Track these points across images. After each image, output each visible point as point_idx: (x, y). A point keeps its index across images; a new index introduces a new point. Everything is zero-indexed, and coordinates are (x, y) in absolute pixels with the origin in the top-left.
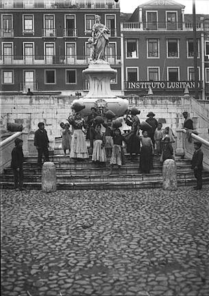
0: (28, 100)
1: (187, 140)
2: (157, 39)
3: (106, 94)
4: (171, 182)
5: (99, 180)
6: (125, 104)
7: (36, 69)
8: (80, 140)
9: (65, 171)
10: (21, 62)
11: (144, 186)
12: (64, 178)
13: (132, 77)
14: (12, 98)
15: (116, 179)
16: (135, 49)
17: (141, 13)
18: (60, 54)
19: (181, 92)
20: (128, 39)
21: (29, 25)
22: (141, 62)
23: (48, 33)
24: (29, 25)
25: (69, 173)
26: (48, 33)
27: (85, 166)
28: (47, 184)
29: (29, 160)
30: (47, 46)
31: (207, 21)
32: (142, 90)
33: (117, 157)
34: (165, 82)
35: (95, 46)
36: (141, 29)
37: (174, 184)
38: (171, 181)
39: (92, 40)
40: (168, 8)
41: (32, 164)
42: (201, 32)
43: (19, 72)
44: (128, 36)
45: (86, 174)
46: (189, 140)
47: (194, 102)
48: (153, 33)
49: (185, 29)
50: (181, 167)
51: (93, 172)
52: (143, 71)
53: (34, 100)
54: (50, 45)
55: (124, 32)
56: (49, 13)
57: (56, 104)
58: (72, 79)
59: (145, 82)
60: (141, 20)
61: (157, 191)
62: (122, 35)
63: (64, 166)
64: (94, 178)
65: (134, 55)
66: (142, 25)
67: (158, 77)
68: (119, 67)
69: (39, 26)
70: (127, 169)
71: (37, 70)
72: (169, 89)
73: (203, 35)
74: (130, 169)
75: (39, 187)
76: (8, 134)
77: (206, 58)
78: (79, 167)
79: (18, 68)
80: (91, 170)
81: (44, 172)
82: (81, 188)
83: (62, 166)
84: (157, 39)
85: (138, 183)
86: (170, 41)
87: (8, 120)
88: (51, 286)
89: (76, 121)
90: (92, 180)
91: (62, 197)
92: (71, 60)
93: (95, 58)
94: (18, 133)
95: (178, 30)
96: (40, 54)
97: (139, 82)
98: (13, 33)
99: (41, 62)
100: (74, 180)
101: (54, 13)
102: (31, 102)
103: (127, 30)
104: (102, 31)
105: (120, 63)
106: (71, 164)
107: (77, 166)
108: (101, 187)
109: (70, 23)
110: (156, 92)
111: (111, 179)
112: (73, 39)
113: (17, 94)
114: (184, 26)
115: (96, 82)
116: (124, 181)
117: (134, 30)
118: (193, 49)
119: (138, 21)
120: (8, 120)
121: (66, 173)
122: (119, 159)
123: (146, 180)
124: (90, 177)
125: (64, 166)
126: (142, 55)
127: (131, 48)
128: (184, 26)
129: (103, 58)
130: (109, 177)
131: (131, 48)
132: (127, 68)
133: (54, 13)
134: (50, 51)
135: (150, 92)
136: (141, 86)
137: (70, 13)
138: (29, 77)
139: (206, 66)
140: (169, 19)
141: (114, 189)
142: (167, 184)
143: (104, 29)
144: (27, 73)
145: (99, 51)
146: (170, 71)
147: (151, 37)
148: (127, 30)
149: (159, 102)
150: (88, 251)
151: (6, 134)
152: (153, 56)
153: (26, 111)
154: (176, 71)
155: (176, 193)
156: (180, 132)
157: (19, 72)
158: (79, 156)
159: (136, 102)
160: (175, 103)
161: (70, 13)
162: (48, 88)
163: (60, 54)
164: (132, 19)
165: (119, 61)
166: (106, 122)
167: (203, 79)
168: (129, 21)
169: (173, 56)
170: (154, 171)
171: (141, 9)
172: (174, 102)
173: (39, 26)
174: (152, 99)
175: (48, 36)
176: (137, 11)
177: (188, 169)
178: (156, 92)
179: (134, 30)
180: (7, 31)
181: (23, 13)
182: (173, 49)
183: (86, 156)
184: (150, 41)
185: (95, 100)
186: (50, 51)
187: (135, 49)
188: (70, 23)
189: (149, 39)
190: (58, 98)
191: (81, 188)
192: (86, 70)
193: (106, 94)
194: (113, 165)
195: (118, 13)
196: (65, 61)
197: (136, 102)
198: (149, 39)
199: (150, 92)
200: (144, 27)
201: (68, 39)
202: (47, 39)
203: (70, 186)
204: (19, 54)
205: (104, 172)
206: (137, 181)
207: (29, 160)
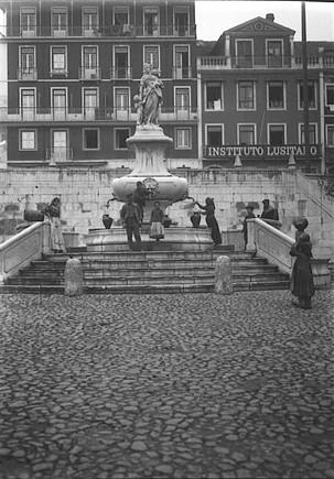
0: (57, 175)
3: (158, 171)
6: (183, 185)
9: (96, 271)
10: (47, 117)
11: (193, 290)
12: (95, 280)
13: (214, 138)
14: (34, 173)
16: (219, 97)
17: (228, 42)
18: (106, 104)
19: (284, 161)
20: (207, 82)
21: (59, 62)
23: (88, 73)
24: (59, 62)
26: (88, 73)
28: (71, 286)
29: (52, 259)
30: (87, 92)
31: (329, 54)
34: (264, 147)
35: (144, 105)
36: (228, 67)
40: (269, 34)
41: (56, 263)
42: (318, 71)
43: (44, 131)
44: (209, 78)
45: (123, 275)
47: (300, 177)
48: (246, 73)
49: (294, 66)
50: (248, 268)
53: (65, 175)
54: (91, 92)
55: (202, 72)
56: (88, 43)
57: (97, 180)
58: (91, 142)
60: (227, 53)
62: (199, 76)
64: (132, 279)
65: (218, 106)
66: (229, 61)
67: (254, 138)
69: (74, 65)
71: (72, 129)
73: (321, 75)
74: (179, 270)
75: (62, 291)
76: (25, 224)
77: (327, 110)
79: (44, 127)
81: (68, 270)
82: (115, 291)
85: (188, 286)
87: (27, 203)
88: (64, 405)
92: (122, 115)
94: (38, 223)
95: (285, 67)
96: (75, 104)
97: (225, 146)
98: (36, 74)
99: (79, 117)
101: (96, 43)
102: (61, 178)
103: (207, 68)
109: (122, 59)
110: (246, 161)
112: (125, 83)
113: (41, 165)
114: (293, 61)
117: (218, 68)
118: (309, 95)
119: (224, 54)
120: (27, 203)
124: (127, 280)
126: (229, 103)
127: (213, 95)
128: (293, 61)
131: (213, 95)
132: (206, 125)
133: (96, 43)
134: (91, 101)
135: (238, 162)
138: (60, 140)
139: (327, 121)
140: (271, 51)
142: (219, 287)
144: (56, 134)
145: (150, 111)
147: (241, 79)
148: (207, 68)
149: (248, 177)
150: (98, 340)
151: (22, 225)
152: (247, 107)
154: (281, 129)
162: (88, 155)
163: (106, 104)
164: (214, 50)
165: (194, 114)
167: (323, 141)
171: (228, 37)
172: (270, 177)
173: (74, 65)
174: (238, 172)
175: (88, 78)
176: (222, 38)
177: (257, 271)
178: (246, 161)
179: (218, 68)
180: (27, 71)
181: (52, 44)
182: (276, 96)
184: (242, 84)
186: (91, 101)
187: (219, 97)
188: (122, 59)
190: (101, 172)
191: (115, 291)
193: (158, 171)
195: (193, 42)
196: (113, 115)
199: (238, 162)
200: (233, 63)
201: (118, 83)
204: (44, 104)
207: (52, 259)
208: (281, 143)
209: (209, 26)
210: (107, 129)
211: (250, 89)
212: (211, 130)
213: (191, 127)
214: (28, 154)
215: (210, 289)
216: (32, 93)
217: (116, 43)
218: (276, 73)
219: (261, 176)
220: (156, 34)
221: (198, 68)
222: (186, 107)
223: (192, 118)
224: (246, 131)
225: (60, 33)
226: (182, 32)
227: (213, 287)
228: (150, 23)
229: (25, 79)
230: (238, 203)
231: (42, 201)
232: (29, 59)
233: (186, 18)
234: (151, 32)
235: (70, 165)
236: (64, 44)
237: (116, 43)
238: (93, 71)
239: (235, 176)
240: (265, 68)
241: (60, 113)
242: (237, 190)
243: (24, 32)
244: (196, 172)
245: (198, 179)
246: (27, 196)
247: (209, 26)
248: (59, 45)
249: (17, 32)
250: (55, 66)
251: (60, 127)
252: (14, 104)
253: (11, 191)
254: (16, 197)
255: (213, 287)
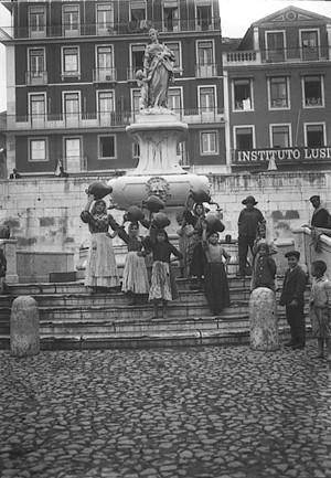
1: (313, 248)
2: (286, 77)
4: (266, 333)
5: (131, 328)
7: (85, 135)
8: (102, 252)
9: (71, 311)
10: (59, 124)
11: (217, 342)
13: (244, 142)
15: (163, 327)
16: (249, 96)
17: (256, 36)
20: (235, 79)
21: (72, 64)
22: (260, 116)
24: (72, 64)
25: (78, 316)
27: (111, 302)
28: (21, 341)
30: (102, 96)
32: (261, 162)
33: (162, 284)
34: (301, 149)
35: (149, 82)
36: (258, 62)
37: (271, 338)
38: (264, 332)
39: (145, 73)
40: (303, 24)
43: (56, 140)
44: (235, 75)
45: (110, 317)
46: (316, 249)
48: (278, 68)
51: (124, 314)
52: (263, 132)
53: (72, 185)
54: (106, 96)
55: (228, 69)
56: (104, 42)
58: (108, 150)
59: (266, 149)
60: (256, 47)
61: (235, 352)
62: (225, 73)
63: (73, 303)
65: (247, 105)
66: (258, 56)
67: (289, 141)
68: (222, 126)
69: (88, 65)
70: (188, 308)
71: (86, 136)
72: (308, 160)
78: (99, 303)
79: (56, 135)
80: (120, 310)
83: (68, 302)
84: (286, 77)
85: (206, 334)
86: (308, 79)
89: (96, 217)
90: (118, 329)
91: (44, 361)
93: (149, 103)
95: (322, 60)
96: (89, 110)
97: (257, 150)
98: (46, 79)
99: (92, 123)
100: (83, 330)
102: (67, 188)
103: (234, 64)
104: (161, 57)
105: (222, 119)
106: (84, 298)
107: (97, 302)
108: (134, 344)
111: (155, 328)
115: (151, 147)
116: (181, 331)
117: (246, 63)
119: (252, 48)
121: (74, 316)
122: (166, 288)
123: (223, 329)
125: (73, 303)
126: (260, 103)
127: (241, 94)
129: (163, 104)
130: (150, 323)
131: (241, 94)
132: (235, 127)
134: (106, 105)
135: (272, 166)
136: (259, 157)
137: (138, 41)
138: (73, 149)
140: (306, 43)
141: (156, 347)
142: (257, 337)
143: (165, 53)
144: (34, 144)
145: (158, 90)
146: (310, 130)
147: (274, 74)
148: (234, 64)
152: (279, 106)
153: (58, 204)
154: (318, 129)
155: (274, 357)
156: (300, 233)
157: (56, 140)
158: (101, 283)
159: (246, 185)
160: (315, 183)
161: (138, 41)
162: (103, 165)
164: (243, 46)
165: (221, 116)
166: (147, 218)
168: (238, 50)
169: (313, 104)
170: (232, 310)
172: (312, 181)
173: (88, 65)
175: (103, 80)
176: (250, 32)
179: (246, 63)
180: (36, 75)
183: (113, 284)
184: (273, 80)
185: (145, 179)
186: (106, 105)
187: (249, 96)
189: (271, 77)
192: (128, 127)
194: (156, 301)
197: (246, 185)
198: (271, 77)
199: (272, 166)
200: (263, 58)
202: (102, 86)
203: (73, 342)
204: (56, 110)
205: (145, 313)
206: (206, 331)
208: (320, 145)
209: (233, 26)
210: (122, 134)
211: (284, 86)
212: (240, 132)
213: (218, 130)
214: (39, 166)
215: (242, 339)
216: (41, 98)
217: (133, 41)
218: (312, 66)
219: (301, 180)
220: (176, 29)
221: (224, 65)
222: (211, 108)
223: (218, 120)
224: (279, 132)
225: (72, 33)
226: (205, 25)
227: (247, 334)
228: (170, 17)
229: (34, 84)
230: (274, 213)
231: (46, 215)
232: (39, 62)
233: (208, 16)
234: (170, 27)
235: (83, 175)
236: (75, 44)
237: (133, 41)
238: (108, 73)
239: (270, 180)
240: (299, 61)
241: (73, 118)
242: (272, 197)
243: (33, 33)
244: (224, 178)
245: (226, 186)
246: (28, 209)
247: (233, 26)
248: (71, 44)
249: (26, 34)
250: (67, 68)
251: (72, 134)
252: (22, 110)
253: (9, 205)
254: (16, 211)
255: (247, 334)
